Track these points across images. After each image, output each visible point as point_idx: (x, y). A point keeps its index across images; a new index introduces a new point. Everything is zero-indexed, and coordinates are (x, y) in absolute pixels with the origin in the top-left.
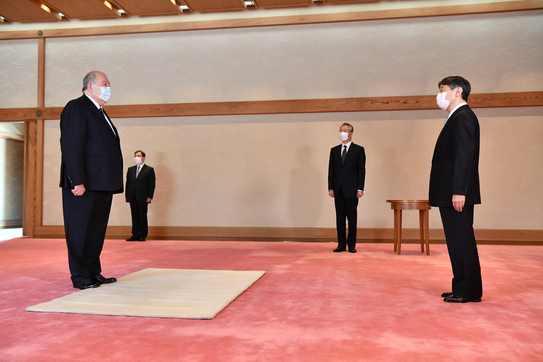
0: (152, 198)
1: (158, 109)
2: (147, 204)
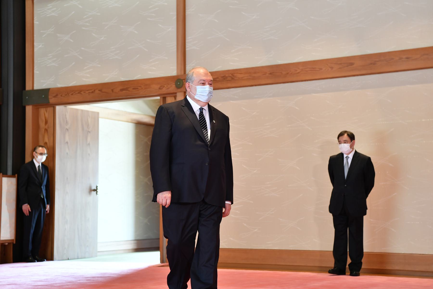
1: (352, 64)
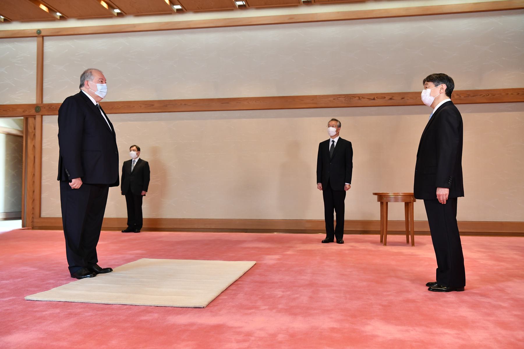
0: (146, 191)
1: (153, 105)
2: (142, 196)
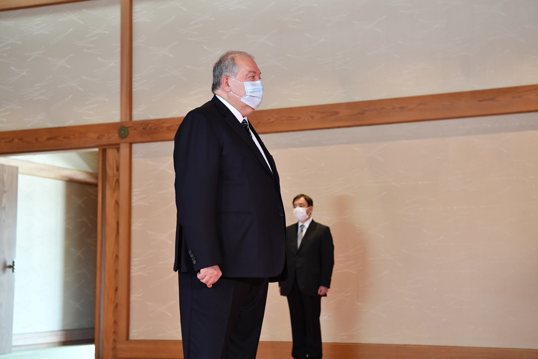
0: (328, 286)
1: (336, 113)
2: (319, 297)
